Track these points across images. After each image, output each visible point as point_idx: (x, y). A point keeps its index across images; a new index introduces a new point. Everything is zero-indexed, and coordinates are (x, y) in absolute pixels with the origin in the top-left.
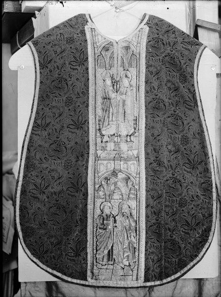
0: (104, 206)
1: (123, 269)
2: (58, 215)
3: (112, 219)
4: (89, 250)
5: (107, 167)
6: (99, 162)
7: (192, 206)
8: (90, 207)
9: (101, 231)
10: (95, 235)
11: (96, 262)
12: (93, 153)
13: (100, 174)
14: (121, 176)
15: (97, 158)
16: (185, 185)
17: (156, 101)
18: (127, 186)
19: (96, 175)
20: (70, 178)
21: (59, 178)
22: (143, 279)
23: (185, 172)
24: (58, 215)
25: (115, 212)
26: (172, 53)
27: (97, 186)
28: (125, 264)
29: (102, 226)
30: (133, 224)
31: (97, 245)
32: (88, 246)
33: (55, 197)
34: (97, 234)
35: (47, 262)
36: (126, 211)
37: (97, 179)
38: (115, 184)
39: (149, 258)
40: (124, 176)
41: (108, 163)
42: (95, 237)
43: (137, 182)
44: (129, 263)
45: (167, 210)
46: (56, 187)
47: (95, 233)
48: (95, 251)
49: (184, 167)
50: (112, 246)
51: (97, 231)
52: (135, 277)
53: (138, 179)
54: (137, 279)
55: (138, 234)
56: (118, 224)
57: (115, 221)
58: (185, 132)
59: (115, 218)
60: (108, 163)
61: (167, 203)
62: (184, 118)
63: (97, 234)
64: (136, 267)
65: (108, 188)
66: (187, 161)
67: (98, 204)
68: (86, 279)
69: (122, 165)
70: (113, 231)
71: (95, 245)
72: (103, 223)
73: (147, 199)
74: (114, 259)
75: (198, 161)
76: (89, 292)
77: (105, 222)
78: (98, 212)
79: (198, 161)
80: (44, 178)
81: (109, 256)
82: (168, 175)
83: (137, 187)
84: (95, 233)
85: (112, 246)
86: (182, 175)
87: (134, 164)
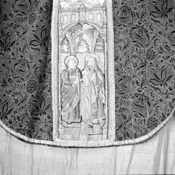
0: (69, 60)
1: (92, 127)
2: (23, 71)
3: (78, 74)
4: (54, 108)
5: (71, 18)
6: (63, 14)
7: (162, 59)
8: (54, 62)
9: (66, 87)
10: (60, 91)
11: (62, 120)
12: (57, 4)
13: (63, 27)
14: (86, 27)
15: (60, 9)
16: (153, 35)
17: (138, 98)
18: (93, 37)
19: (60, 28)
20: (34, 31)
21: (24, 33)
22: (114, 137)
23: (152, 22)
24: (23, 71)
25: (81, 67)
26: (141, 25)
27: (61, 40)
28: (94, 122)
29: (67, 82)
30: (101, 78)
31: (62, 102)
32: (53, 103)
33: (20, 53)
34: (62, 90)
35: (10, 122)
36: (92, 64)
37: (60, 32)
38: (81, 35)
39: (121, 115)
40: (89, 27)
41: (72, 15)
42: (60, 93)
43: (105, 33)
44: (98, 121)
45: (134, 60)
46: (20, 42)
47: (60, 89)
48: (60, 108)
49: (152, 16)
50: (79, 103)
51: (62, 87)
52: (105, 136)
53: (105, 30)
54: (108, 138)
55: (107, 89)
56: (85, 79)
57: (81, 76)
58: (150, 46)
59: (81, 73)
60: (72, 15)
61: (135, 53)
62: (151, 98)
63: (62, 90)
64: (106, 125)
65: (72, 40)
66: (155, 10)
67: (62, 59)
68: (51, 139)
69: (89, 17)
70: (80, 87)
71: (60, 101)
72: (68, 78)
73: (116, 52)
74: (81, 117)
75: (167, 8)
76: (59, 155)
77: (70, 77)
78: (62, 67)
79: (167, 8)
80: (9, 34)
81: (76, 112)
82: (135, 23)
83: (104, 38)
84: (60, 89)
85: (79, 103)
86: (151, 91)
87: (100, 13)
